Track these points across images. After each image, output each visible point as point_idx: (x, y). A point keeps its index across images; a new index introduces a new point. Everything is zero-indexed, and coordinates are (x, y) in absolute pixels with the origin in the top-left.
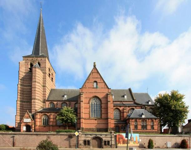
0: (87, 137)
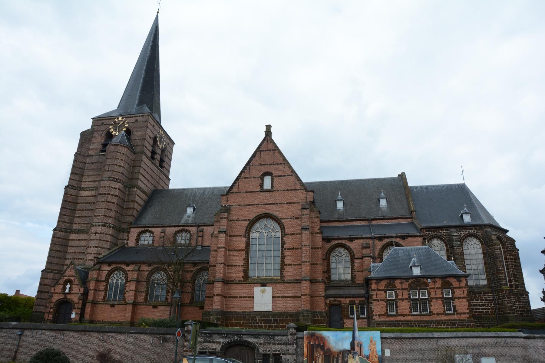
0: (210, 342)
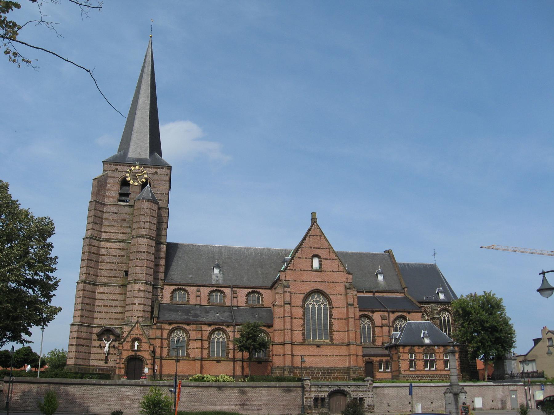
0: (321, 391)
